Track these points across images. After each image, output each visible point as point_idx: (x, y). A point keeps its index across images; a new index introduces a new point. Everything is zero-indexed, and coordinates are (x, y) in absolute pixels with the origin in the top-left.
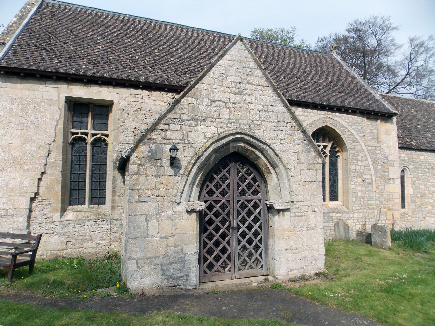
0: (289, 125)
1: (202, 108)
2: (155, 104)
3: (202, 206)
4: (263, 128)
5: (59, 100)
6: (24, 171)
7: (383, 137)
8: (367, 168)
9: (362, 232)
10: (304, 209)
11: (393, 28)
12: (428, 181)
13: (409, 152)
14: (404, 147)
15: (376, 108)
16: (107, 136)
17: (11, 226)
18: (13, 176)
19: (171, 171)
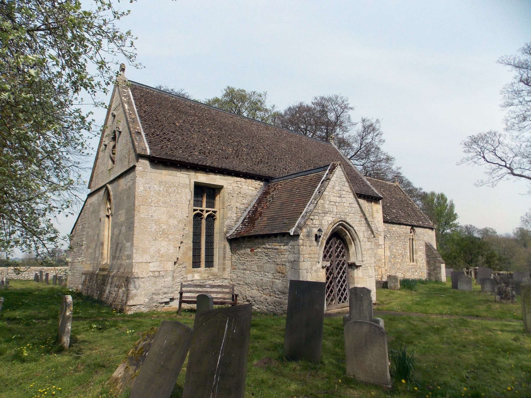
0: (360, 215)
1: (326, 206)
2: (248, 189)
3: (328, 264)
4: (350, 217)
5: (190, 184)
6: (170, 240)
9: (379, 281)
10: (367, 265)
11: (350, 108)
12: (397, 246)
14: (386, 221)
15: (370, 194)
16: (215, 212)
17: (163, 285)
18: (162, 245)
19: (315, 243)
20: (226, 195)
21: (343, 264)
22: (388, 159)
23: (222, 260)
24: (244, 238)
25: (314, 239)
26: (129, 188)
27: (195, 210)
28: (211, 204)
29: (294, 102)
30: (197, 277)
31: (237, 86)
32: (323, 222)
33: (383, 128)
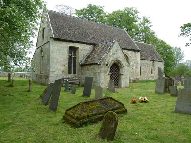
1: (111, 55)
3: (111, 74)
7: (137, 57)
8: (133, 65)
11: (139, 12)
13: (143, 60)
14: (142, 59)
15: (136, 49)
16: (76, 56)
20: (80, 50)
21: (117, 74)
22: (154, 33)
23: (78, 72)
24: (85, 65)
25: (106, 65)
26: (48, 48)
27: (69, 55)
28: (75, 53)
29: (116, 10)
30: (70, 77)
31: (93, 4)
32: (110, 60)
33: (151, 20)
